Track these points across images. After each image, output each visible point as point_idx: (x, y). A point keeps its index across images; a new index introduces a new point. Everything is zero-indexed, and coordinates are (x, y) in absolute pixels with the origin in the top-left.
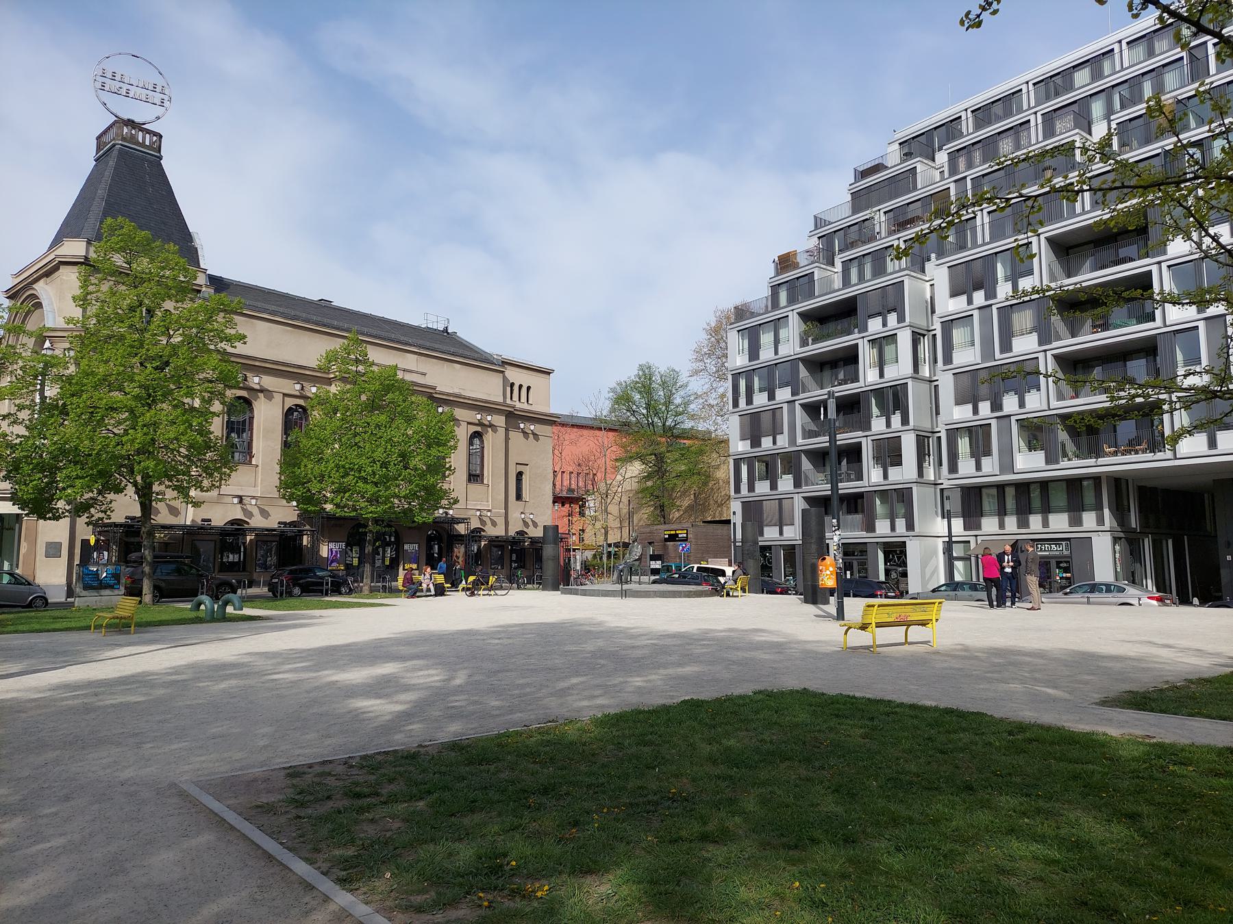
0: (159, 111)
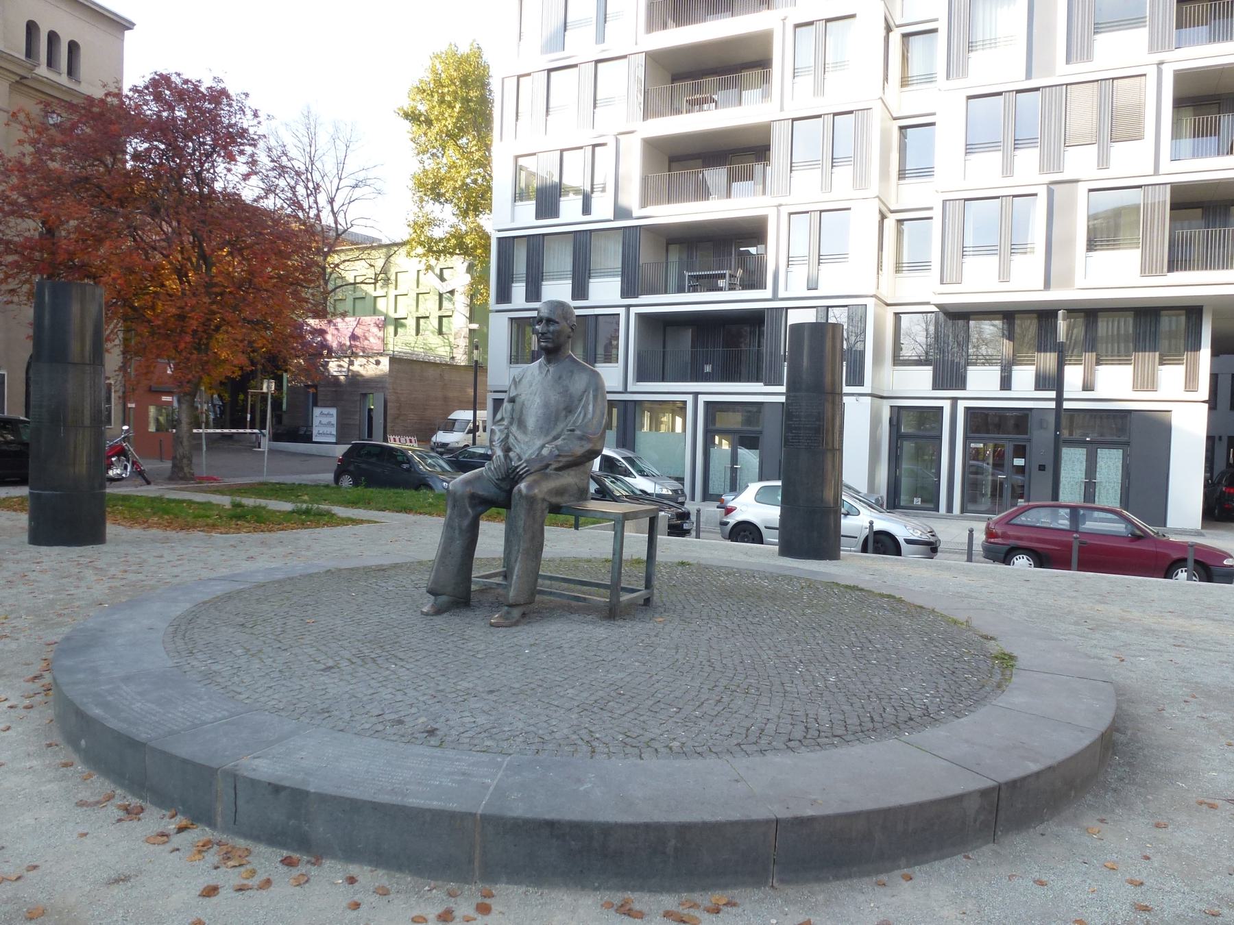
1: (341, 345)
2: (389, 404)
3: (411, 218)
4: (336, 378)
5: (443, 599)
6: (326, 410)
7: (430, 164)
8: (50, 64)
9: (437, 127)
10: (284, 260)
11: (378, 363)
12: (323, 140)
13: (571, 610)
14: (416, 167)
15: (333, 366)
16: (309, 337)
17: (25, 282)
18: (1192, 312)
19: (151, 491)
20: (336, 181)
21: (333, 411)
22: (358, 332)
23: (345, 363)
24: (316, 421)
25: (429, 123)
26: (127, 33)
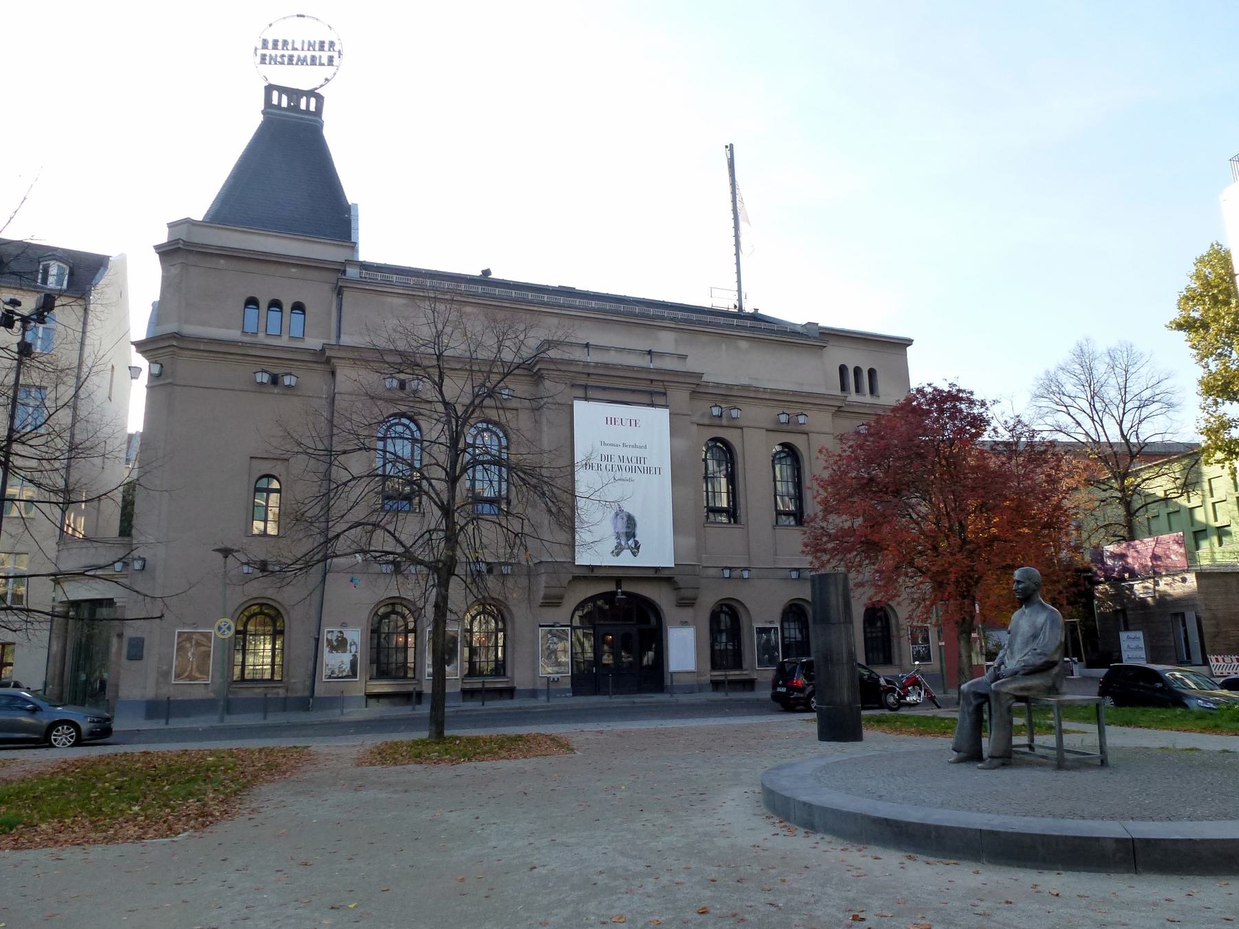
0: (328, 71)
1: (1144, 567)
2: (1204, 622)
3: (1203, 424)
4: (1143, 600)
5: (962, 755)
6: (1132, 634)
7: (1214, 365)
8: (858, 390)
9: (1214, 327)
10: (1198, 445)
11: (1184, 580)
12: (1100, 369)
13: (1040, 765)
14: (1200, 372)
15: (1138, 587)
16: (1110, 562)
17: (841, 560)
19: (941, 713)
20: (1122, 405)
21: (1140, 634)
22: (1158, 551)
23: (1150, 583)
24: (1124, 645)
25: (1205, 326)
26: (908, 349)
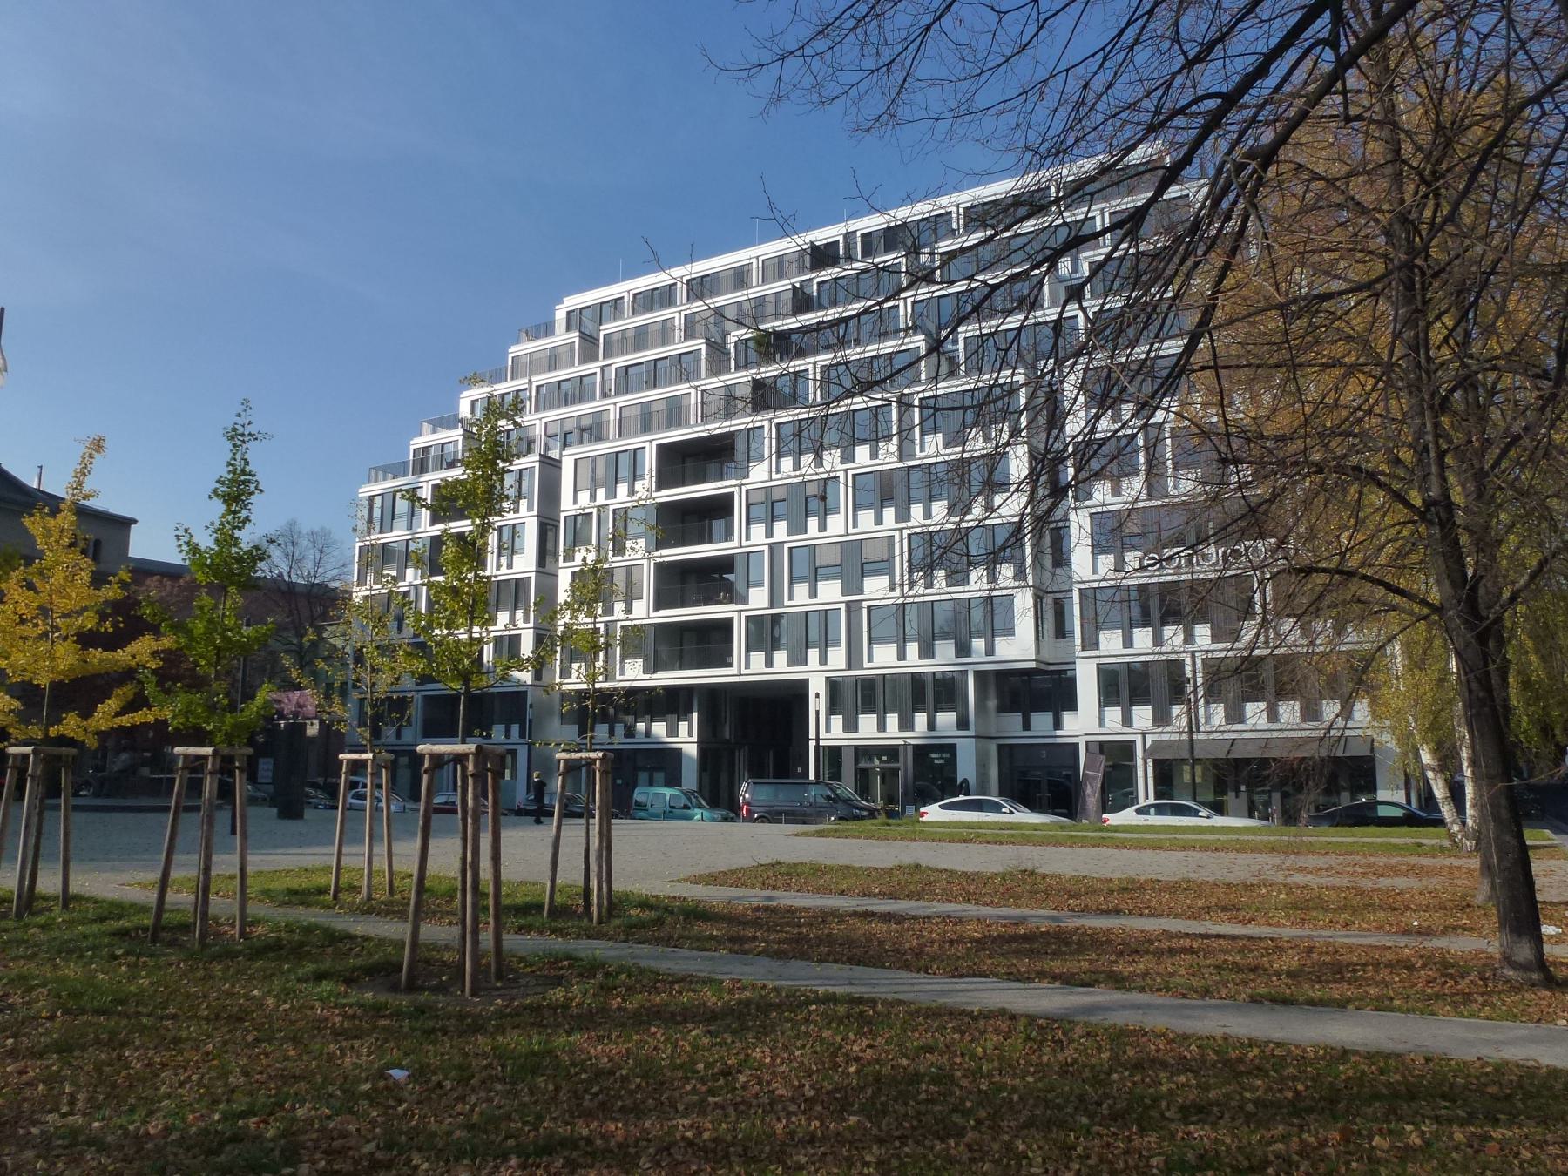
18: (690, 689)
